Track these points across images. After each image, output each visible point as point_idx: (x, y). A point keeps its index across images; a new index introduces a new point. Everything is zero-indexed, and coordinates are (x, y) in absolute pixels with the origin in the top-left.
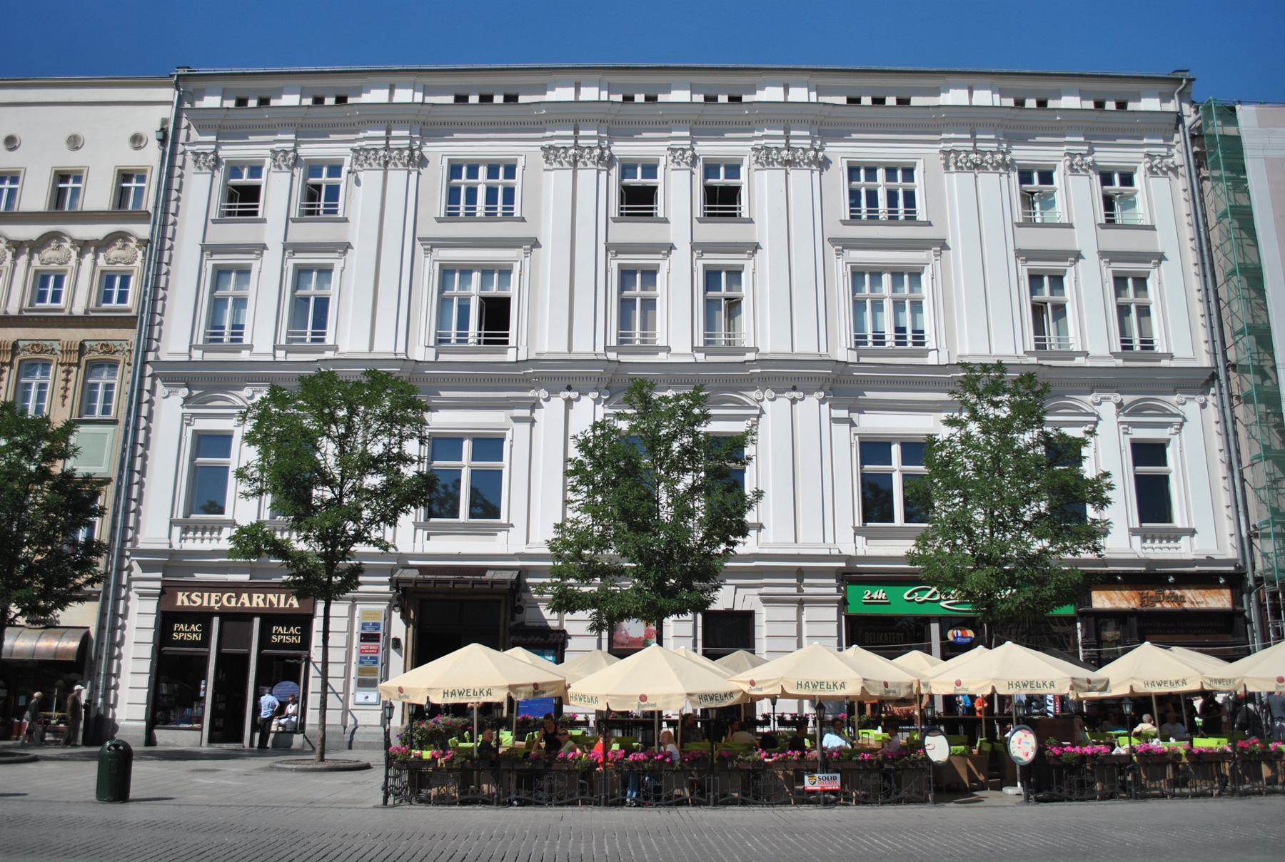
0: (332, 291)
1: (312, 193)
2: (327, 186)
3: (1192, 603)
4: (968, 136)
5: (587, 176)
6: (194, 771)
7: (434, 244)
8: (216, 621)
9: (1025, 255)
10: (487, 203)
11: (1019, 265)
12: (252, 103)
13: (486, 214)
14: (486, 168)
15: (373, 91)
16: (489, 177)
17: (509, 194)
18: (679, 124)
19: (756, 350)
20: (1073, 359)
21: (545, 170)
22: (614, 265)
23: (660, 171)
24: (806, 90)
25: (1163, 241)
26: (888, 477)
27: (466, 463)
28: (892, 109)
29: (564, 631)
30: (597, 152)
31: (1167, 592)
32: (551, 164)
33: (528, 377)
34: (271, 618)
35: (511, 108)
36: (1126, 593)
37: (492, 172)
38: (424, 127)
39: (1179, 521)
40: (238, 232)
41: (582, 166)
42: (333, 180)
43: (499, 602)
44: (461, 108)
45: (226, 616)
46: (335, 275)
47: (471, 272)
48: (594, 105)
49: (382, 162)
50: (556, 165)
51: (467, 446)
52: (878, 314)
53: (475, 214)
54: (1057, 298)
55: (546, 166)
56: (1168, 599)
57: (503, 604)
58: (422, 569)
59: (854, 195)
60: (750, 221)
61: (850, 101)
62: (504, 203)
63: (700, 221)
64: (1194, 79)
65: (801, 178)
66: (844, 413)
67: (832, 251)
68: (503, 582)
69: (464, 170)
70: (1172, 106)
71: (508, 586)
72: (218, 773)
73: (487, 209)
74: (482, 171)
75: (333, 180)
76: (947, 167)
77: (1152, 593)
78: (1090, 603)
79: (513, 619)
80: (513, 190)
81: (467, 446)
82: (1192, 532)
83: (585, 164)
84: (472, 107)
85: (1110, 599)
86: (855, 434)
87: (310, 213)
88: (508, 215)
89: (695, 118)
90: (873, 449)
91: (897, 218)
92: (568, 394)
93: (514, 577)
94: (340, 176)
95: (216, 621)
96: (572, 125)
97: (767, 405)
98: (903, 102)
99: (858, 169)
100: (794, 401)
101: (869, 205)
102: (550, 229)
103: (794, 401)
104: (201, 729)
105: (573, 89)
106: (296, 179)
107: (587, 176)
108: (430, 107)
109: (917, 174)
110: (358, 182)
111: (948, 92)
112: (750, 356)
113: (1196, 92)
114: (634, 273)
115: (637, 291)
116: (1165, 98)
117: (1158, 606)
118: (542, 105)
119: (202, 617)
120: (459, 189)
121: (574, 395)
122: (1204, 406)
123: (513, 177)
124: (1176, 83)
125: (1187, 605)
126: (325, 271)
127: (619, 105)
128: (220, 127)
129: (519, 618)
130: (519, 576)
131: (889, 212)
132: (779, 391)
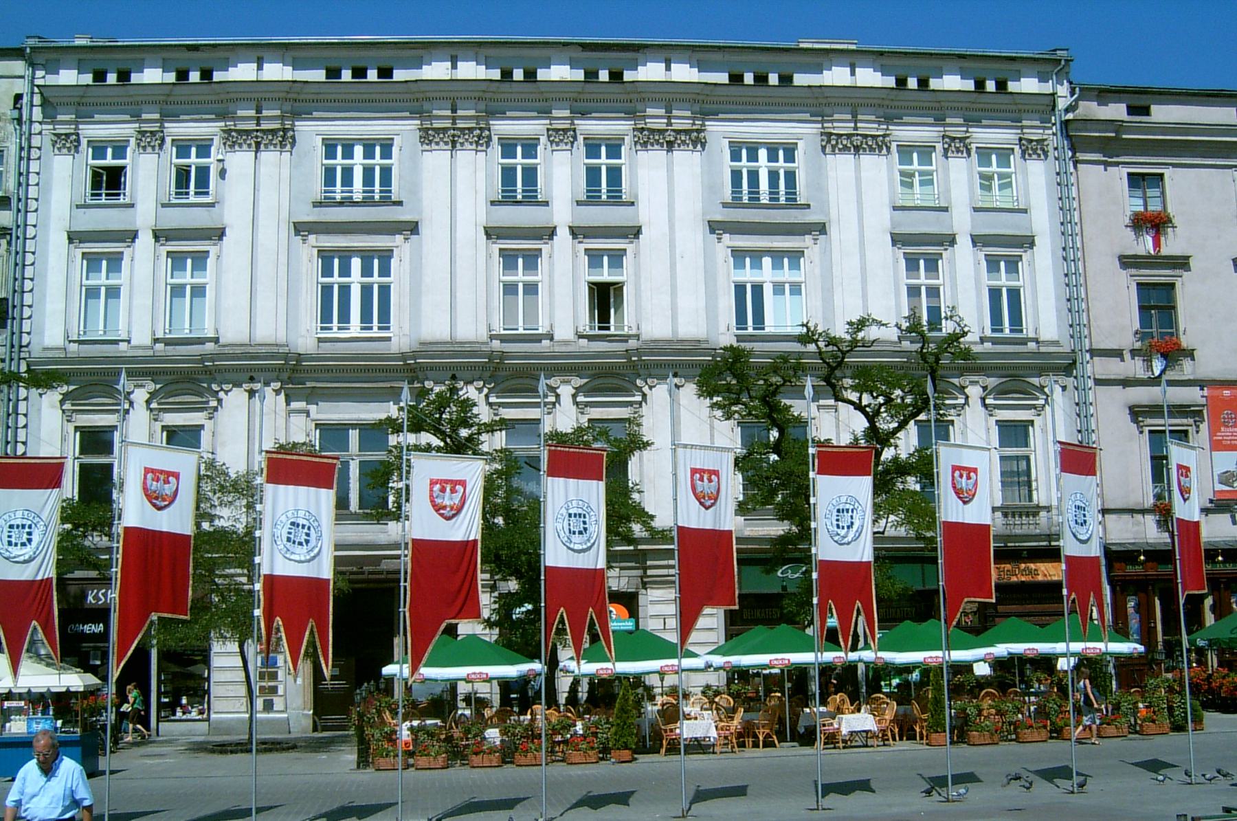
1: (182, 176)
2: (197, 168)
3: (1045, 575)
4: (448, 113)
6: (271, 808)
13: (588, 197)
18: (560, 101)
19: (216, 340)
20: (626, 341)
28: (750, 88)
31: (1023, 566)
38: (79, 108)
40: (105, 218)
44: (735, 90)
51: (354, 435)
53: (621, 197)
56: (1022, 572)
60: (546, 204)
61: (732, 78)
64: (1072, 60)
66: (301, 405)
70: (1047, 88)
72: (459, 801)
73: (588, 191)
76: (824, 148)
77: (1008, 567)
81: (354, 435)
84: (192, 87)
86: (77, 428)
88: (386, 201)
89: (575, 95)
92: (676, 380)
96: (254, 104)
98: (786, 80)
99: (777, 150)
109: (799, 154)
111: (430, 64)
113: (1075, 72)
116: (1043, 79)
117: (1014, 579)
120: (335, 169)
124: (1050, 66)
125: (1040, 578)
131: (364, 192)
132: (663, 378)
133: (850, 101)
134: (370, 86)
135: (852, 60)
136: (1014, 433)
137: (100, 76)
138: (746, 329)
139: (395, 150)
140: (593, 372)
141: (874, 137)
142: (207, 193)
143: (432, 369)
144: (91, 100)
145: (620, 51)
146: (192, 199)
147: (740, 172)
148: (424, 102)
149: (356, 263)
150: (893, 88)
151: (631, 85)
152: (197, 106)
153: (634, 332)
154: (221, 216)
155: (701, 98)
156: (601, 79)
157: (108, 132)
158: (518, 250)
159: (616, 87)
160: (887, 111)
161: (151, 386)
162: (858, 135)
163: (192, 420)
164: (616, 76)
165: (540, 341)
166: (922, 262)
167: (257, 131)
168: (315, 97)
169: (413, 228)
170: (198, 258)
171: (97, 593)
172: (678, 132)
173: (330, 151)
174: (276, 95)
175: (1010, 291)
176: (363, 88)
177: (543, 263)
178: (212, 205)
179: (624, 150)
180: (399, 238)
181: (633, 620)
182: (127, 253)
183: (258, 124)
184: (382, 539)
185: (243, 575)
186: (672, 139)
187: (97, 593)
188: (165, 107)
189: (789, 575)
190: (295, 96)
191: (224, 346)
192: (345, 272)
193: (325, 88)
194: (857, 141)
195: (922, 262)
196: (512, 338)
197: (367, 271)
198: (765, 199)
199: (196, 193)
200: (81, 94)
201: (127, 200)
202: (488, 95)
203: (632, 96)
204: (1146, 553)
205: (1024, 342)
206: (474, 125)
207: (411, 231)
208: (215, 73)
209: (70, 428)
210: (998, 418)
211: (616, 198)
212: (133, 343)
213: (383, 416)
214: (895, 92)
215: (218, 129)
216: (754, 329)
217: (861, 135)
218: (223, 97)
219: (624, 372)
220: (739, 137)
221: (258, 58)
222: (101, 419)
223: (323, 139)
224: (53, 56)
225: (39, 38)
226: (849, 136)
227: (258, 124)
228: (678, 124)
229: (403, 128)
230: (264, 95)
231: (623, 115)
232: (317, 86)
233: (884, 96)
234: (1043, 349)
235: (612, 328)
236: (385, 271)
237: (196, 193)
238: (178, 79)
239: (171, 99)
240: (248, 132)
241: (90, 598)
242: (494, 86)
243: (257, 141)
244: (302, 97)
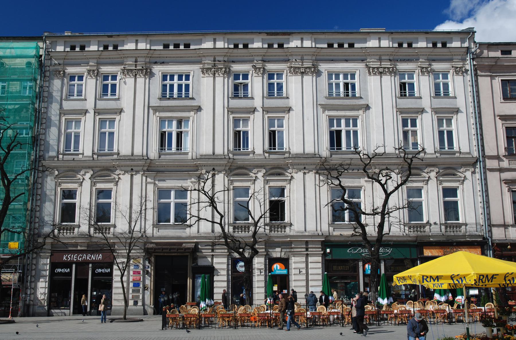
0: (115, 130)
5: (219, 80)
7: (156, 109)
8: (74, 266)
9: (401, 111)
10: (178, 91)
11: (433, 115)
12: (111, 48)
13: (178, 96)
14: (177, 76)
15: (129, 44)
16: (344, 79)
17: (187, 86)
20: (284, 154)
21: (203, 77)
22: (231, 117)
23: (250, 77)
24: (387, 41)
25: (460, 103)
26: (169, 204)
27: (172, 200)
29: (214, 267)
30: (224, 69)
32: (205, 74)
33: (197, 165)
34: (97, 265)
35: (351, 50)
36: (437, 250)
37: (180, 78)
39: (287, 220)
41: (218, 75)
42: (114, 82)
43: (187, 256)
44: (330, 50)
45: (78, 264)
46: (116, 123)
47: (172, 121)
48: (458, 49)
49: (134, 74)
50: (207, 75)
51: (173, 193)
52: (416, 137)
54: (449, 129)
55: (202, 75)
57: (189, 256)
58: (156, 244)
59: (164, 86)
62: (185, 91)
63: (434, 98)
65: (308, 79)
67: (320, 110)
68: (189, 249)
69: (168, 77)
70: (466, 45)
71: (191, 250)
74: (176, 77)
75: (114, 82)
78: (423, 254)
80: (189, 85)
81: (173, 193)
82: (466, 225)
83: (219, 74)
85: (431, 252)
87: (236, 96)
88: (187, 97)
90: (163, 193)
91: (440, 95)
93: (193, 247)
94: (248, 79)
95: (74, 266)
97: (294, 175)
99: (332, 75)
100: (305, 173)
101: (170, 91)
102: (294, 102)
103: (305, 173)
104: (70, 309)
105: (300, 41)
106: (98, 82)
107: (219, 80)
108: (153, 51)
109: (357, 76)
110: (125, 83)
112: (287, 155)
114: (240, 120)
115: (107, 130)
118: (416, 49)
119: (68, 265)
120: (332, 84)
121: (306, 171)
122: (474, 173)
123: (189, 80)
126: (112, 121)
127: (232, 50)
128: (64, 59)
130: (195, 246)
133: (378, 53)
134: (181, 51)
135: (379, 36)
136: (449, 192)
137: (73, 48)
138: (70, 151)
139: (191, 77)
140: (271, 167)
141: (388, 68)
142: (115, 95)
143: (205, 166)
144: (70, 57)
145: (275, 35)
146: (109, 97)
147: (182, 85)
148: (202, 58)
149: (343, 122)
150: (396, 47)
151: (287, 49)
152: (111, 60)
153: (288, 150)
154: (121, 104)
155: (316, 54)
156: (274, 47)
157: (76, 70)
158: (240, 117)
159: (280, 50)
160: (395, 57)
161: (437, 170)
162: (381, 67)
163: (107, 186)
164: (281, 46)
165: (113, 155)
166: (444, 121)
167: (135, 70)
168: (159, 56)
169: (367, 107)
170: (170, 120)
171: (67, 256)
172: (306, 68)
173: (164, 78)
174: (144, 55)
175: (448, 132)
176: (178, 52)
177: (250, 123)
178: (82, 100)
179: (284, 76)
180: (192, 113)
181: (287, 270)
182: (83, 119)
183: (136, 67)
184: (184, 235)
185: (262, 248)
186: (303, 71)
187: (67, 256)
188: (99, 60)
189: (352, 251)
190: (150, 55)
191: (121, 156)
192: (339, 125)
193: (163, 52)
194: (381, 70)
195: (444, 121)
196: (103, 154)
197: (347, 125)
198: (175, 96)
199: (111, 95)
200: (65, 55)
201: (83, 97)
202: (228, 54)
203: (287, 53)
204: (511, 244)
205: (454, 153)
206: (223, 67)
207: (197, 110)
208: (274, 45)
209: (267, 187)
210: (407, 186)
211: (446, 94)
212: (85, 155)
213: (180, 185)
214: (398, 49)
215: (120, 69)
216: (74, 151)
217: (383, 67)
218: (122, 56)
219: (284, 167)
220: (332, 70)
221: (214, 39)
222: (71, 186)
223: (162, 73)
224: (54, 40)
225: (49, 32)
226: (378, 68)
227: (136, 67)
228: (306, 65)
229: (194, 68)
230: (138, 55)
231: (458, 60)
232: (159, 51)
233: (393, 51)
234: (461, 156)
235: (277, 149)
236: (355, 125)
237: (111, 95)
238: (104, 49)
239: (101, 57)
240: (131, 70)
241: (64, 258)
242: (231, 51)
243: (134, 73)
244: (153, 56)
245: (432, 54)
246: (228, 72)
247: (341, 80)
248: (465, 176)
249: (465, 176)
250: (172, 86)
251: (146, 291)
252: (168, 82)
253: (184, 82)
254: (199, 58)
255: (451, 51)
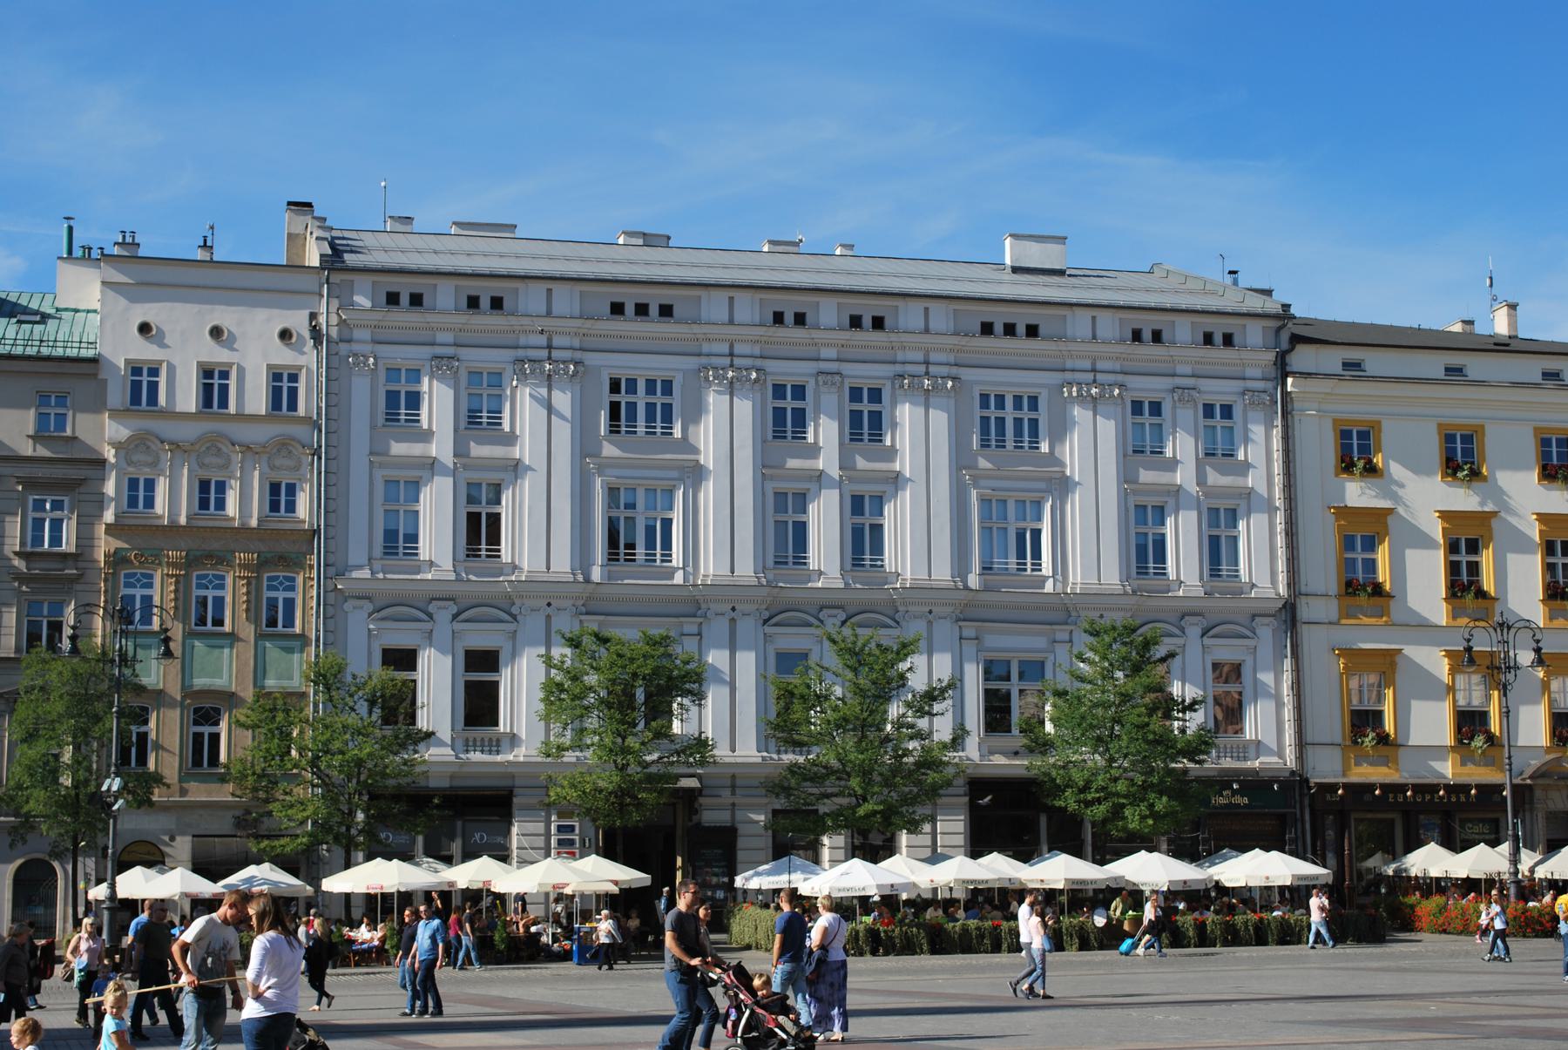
39: (503, 726)
59: (985, 421)
79: (691, 820)
102: (526, 450)
109: (1042, 404)
129: (695, 818)
135: (927, 305)
147: (655, 404)
173: (615, 386)
245: (1203, 360)
246: (580, 373)
247: (641, 399)
248: (1203, 636)
249: (1203, 636)
250: (1001, 422)
251: (459, 904)
252: (993, 413)
253: (659, 399)
254: (814, 348)
255: (813, 336)
